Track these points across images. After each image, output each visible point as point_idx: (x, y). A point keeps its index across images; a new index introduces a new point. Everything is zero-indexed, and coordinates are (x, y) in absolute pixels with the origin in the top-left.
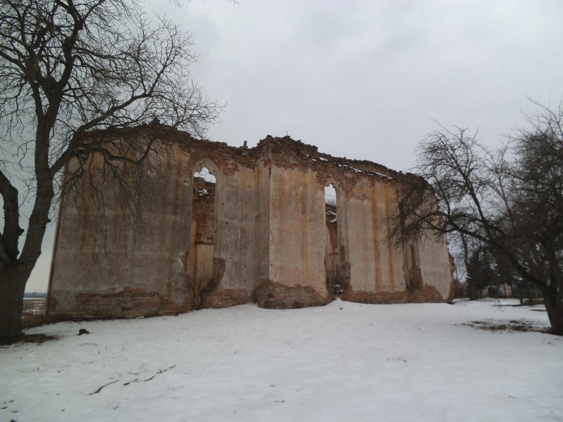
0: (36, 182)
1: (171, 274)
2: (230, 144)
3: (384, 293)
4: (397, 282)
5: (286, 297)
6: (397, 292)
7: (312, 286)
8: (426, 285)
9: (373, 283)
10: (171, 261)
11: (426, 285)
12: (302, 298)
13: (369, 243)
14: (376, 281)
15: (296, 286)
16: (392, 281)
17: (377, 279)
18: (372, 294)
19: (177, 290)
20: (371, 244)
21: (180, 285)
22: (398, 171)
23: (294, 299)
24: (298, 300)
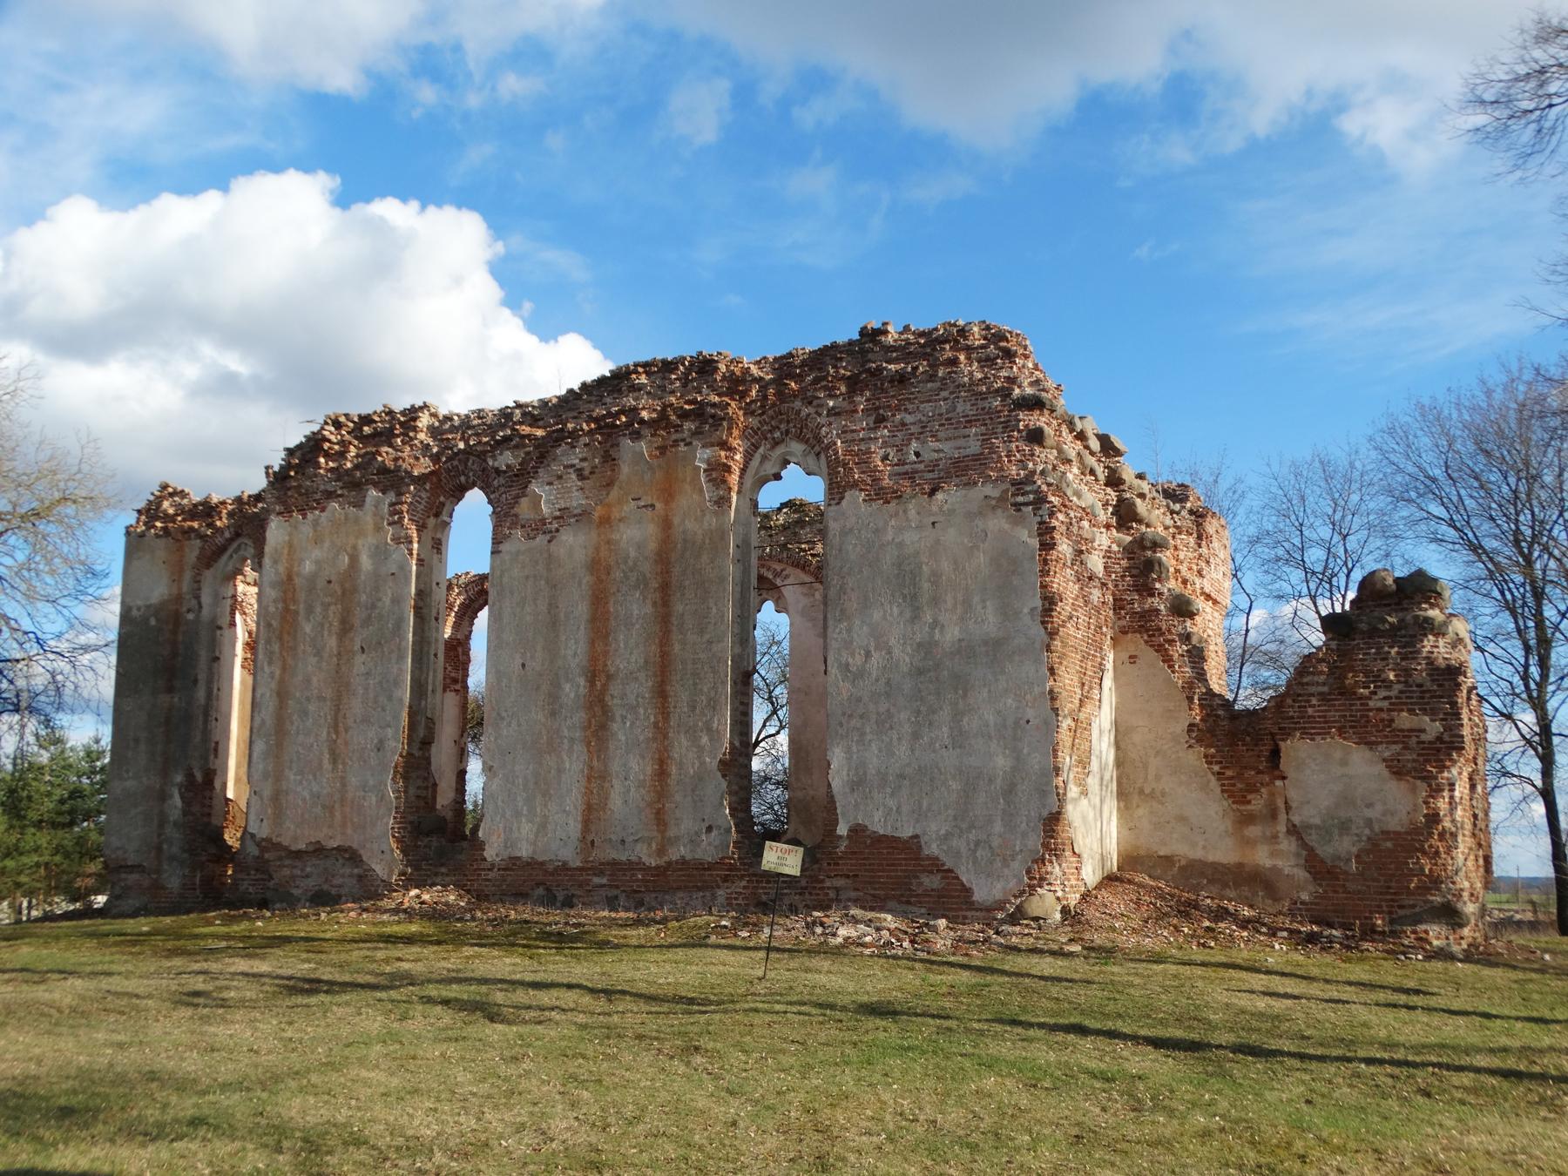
0: (113, 659)
1: (162, 823)
2: (842, 339)
3: (615, 868)
4: (685, 823)
5: (293, 877)
6: (683, 861)
7: (355, 846)
8: (857, 831)
9: (574, 828)
10: (163, 797)
11: (857, 831)
12: (335, 882)
13: (567, 687)
14: (586, 823)
15: (311, 848)
16: (660, 819)
17: (592, 813)
18: (564, 867)
19: (172, 858)
20: (573, 690)
21: (175, 850)
22: (856, 337)
23: (311, 882)
24: (325, 887)
